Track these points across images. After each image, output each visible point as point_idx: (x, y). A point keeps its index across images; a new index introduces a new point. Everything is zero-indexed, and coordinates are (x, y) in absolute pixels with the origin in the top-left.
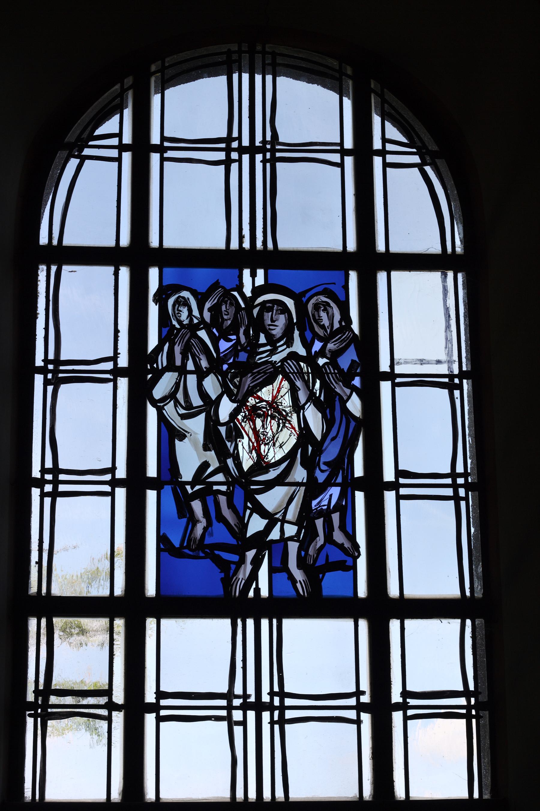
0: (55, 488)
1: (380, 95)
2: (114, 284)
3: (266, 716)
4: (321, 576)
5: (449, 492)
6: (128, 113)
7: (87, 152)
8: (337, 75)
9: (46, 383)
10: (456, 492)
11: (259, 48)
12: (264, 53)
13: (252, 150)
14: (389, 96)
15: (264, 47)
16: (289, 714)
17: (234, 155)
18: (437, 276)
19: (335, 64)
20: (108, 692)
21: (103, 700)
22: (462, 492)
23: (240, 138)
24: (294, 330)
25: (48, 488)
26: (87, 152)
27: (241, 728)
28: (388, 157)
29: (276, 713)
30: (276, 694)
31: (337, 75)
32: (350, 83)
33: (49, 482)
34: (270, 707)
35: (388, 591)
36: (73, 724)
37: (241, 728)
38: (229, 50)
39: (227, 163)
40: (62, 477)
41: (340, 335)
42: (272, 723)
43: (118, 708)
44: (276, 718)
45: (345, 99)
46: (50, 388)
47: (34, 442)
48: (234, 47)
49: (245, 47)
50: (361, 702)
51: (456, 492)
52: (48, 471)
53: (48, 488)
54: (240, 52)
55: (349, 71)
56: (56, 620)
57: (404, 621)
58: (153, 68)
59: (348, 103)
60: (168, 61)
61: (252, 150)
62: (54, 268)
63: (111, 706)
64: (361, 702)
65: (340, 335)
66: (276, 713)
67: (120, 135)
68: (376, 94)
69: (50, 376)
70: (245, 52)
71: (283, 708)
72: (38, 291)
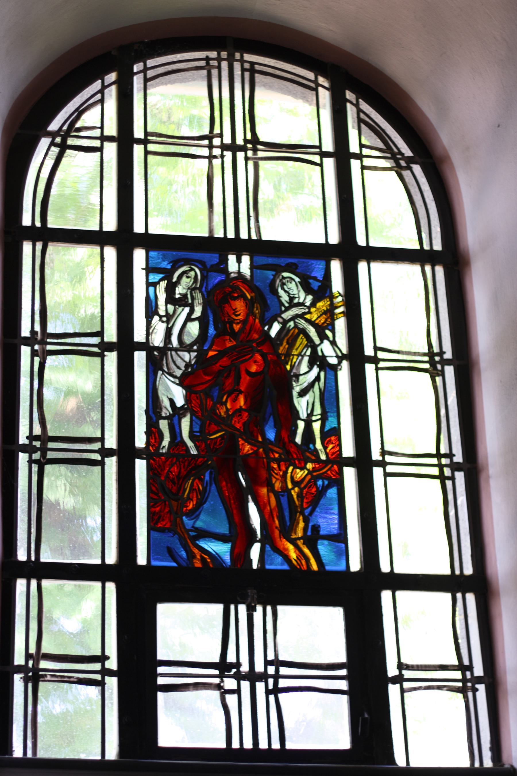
0: (44, 455)
2: (101, 113)
3: (260, 687)
5: (435, 471)
8: (313, 85)
9: (34, 354)
10: (441, 471)
11: (238, 56)
12: (242, 61)
13: (234, 148)
14: (364, 106)
15: (242, 56)
16: (283, 683)
17: (217, 152)
18: (416, 268)
19: (311, 75)
20: (103, 658)
22: (447, 472)
23: (221, 135)
24: (248, 502)
25: (36, 456)
27: (235, 696)
28: (364, 159)
29: (271, 681)
31: (313, 85)
34: (264, 677)
36: (61, 417)
37: (235, 696)
38: (207, 57)
39: (211, 157)
40: (51, 445)
42: (268, 692)
43: (111, 673)
44: (271, 687)
46: (37, 360)
47: (40, 736)
48: (213, 54)
49: (224, 54)
51: (441, 471)
52: (37, 438)
54: (219, 59)
58: (136, 68)
60: (150, 63)
61: (234, 148)
63: (106, 672)
66: (271, 681)
68: (351, 103)
69: (36, 347)
70: (224, 60)
71: (277, 677)
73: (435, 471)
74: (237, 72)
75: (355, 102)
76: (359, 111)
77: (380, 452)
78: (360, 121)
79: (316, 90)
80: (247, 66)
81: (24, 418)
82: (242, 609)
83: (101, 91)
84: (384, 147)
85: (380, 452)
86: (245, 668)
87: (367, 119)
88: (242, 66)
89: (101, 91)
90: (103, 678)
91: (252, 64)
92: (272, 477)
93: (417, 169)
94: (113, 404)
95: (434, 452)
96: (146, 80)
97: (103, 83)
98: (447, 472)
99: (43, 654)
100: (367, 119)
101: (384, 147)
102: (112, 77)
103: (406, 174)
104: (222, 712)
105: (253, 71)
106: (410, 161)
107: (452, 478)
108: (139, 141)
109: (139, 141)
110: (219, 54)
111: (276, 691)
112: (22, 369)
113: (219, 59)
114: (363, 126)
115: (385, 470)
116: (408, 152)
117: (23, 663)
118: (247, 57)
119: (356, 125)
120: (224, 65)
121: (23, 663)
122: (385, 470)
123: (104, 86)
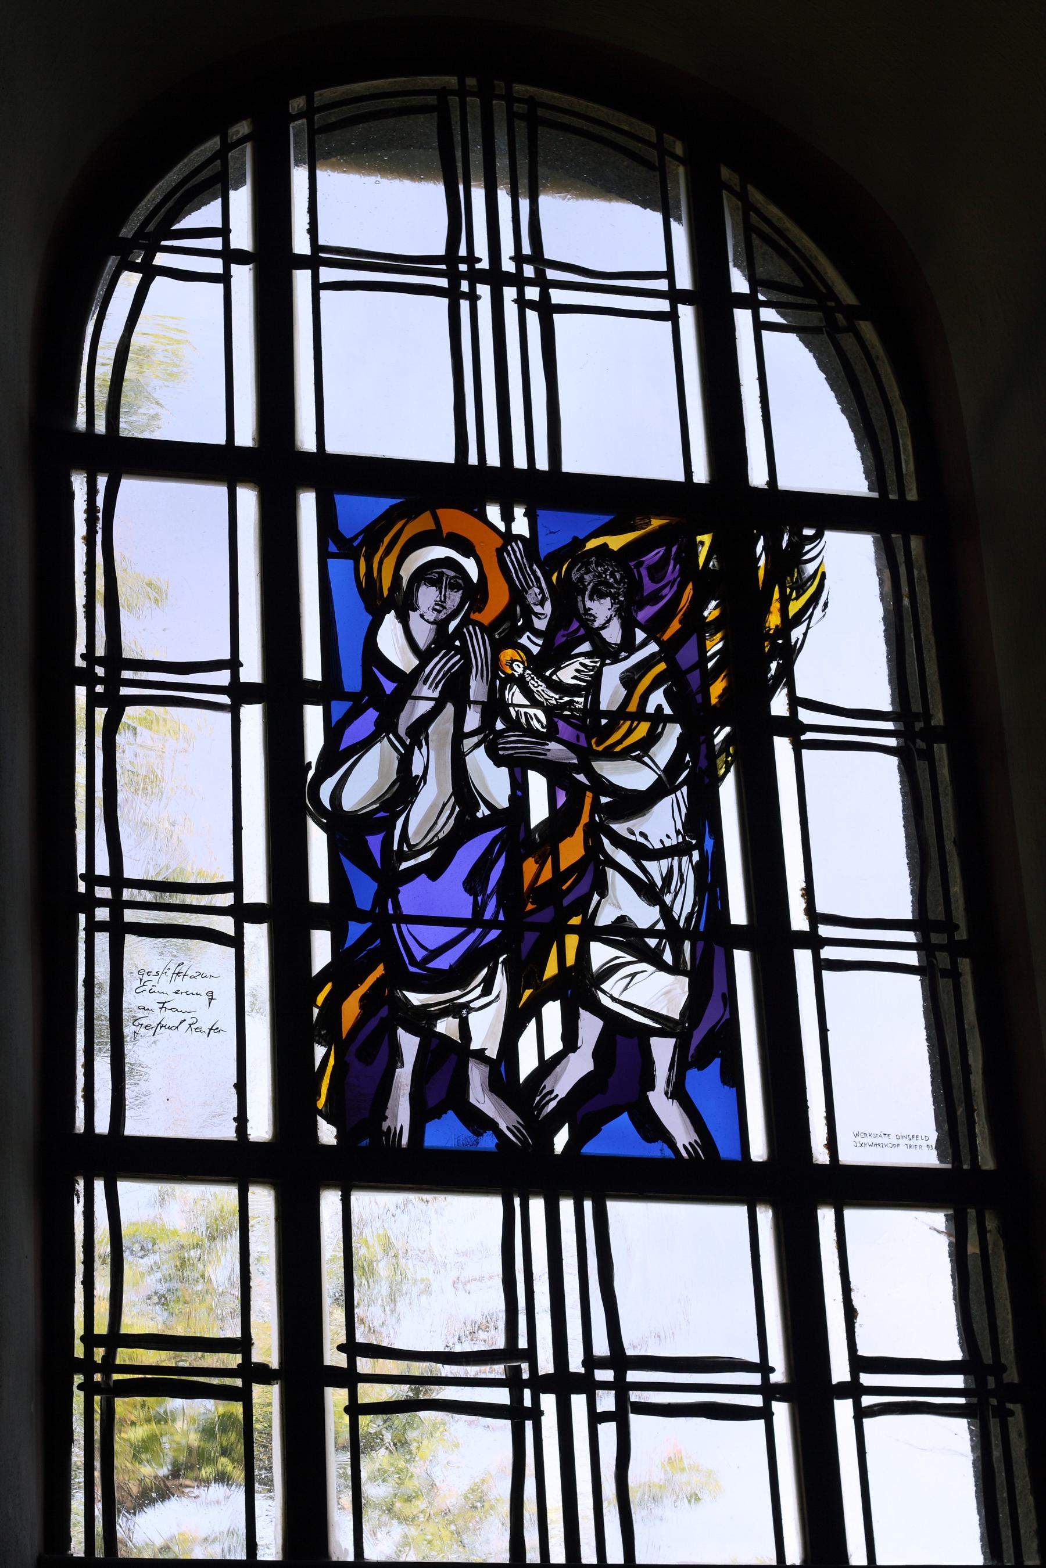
1: (742, 196)
3: (546, 1364)
4: (622, 722)
6: (241, 199)
7: (161, 259)
11: (500, 86)
12: (510, 99)
14: (756, 196)
15: (509, 89)
19: (649, 132)
21: (234, 1360)
26: (161, 259)
30: (464, 296)
32: (681, 170)
33: (103, 902)
35: (750, 478)
40: (127, 894)
41: (697, 962)
45: (674, 225)
50: (670, 322)
53: (102, 914)
54: (462, 92)
55: (679, 150)
56: (97, 1037)
57: (818, 1165)
59: (680, 233)
62: (102, 481)
64: (670, 322)
65: (697, 962)
67: (224, 232)
68: (731, 190)
72: (85, 610)
74: (511, 311)
75: (738, 189)
76: (748, 207)
78: (748, 231)
80: (519, 108)
81: (523, 1336)
83: (222, 154)
84: (797, 283)
86: (546, 1364)
87: (767, 229)
88: (510, 109)
89: (222, 154)
90: (352, 1362)
91: (532, 102)
92: (611, 873)
93: (866, 328)
96: (312, 132)
97: (224, 140)
100: (767, 229)
101: (797, 283)
104: (721, 1015)
105: (534, 123)
106: (852, 314)
108: (302, 262)
109: (302, 262)
110: (462, 82)
111: (509, 1353)
113: (462, 92)
114: (756, 241)
116: (848, 297)
117: (847, 1378)
118: (519, 89)
120: (474, 103)
121: (847, 1378)
123: (227, 147)
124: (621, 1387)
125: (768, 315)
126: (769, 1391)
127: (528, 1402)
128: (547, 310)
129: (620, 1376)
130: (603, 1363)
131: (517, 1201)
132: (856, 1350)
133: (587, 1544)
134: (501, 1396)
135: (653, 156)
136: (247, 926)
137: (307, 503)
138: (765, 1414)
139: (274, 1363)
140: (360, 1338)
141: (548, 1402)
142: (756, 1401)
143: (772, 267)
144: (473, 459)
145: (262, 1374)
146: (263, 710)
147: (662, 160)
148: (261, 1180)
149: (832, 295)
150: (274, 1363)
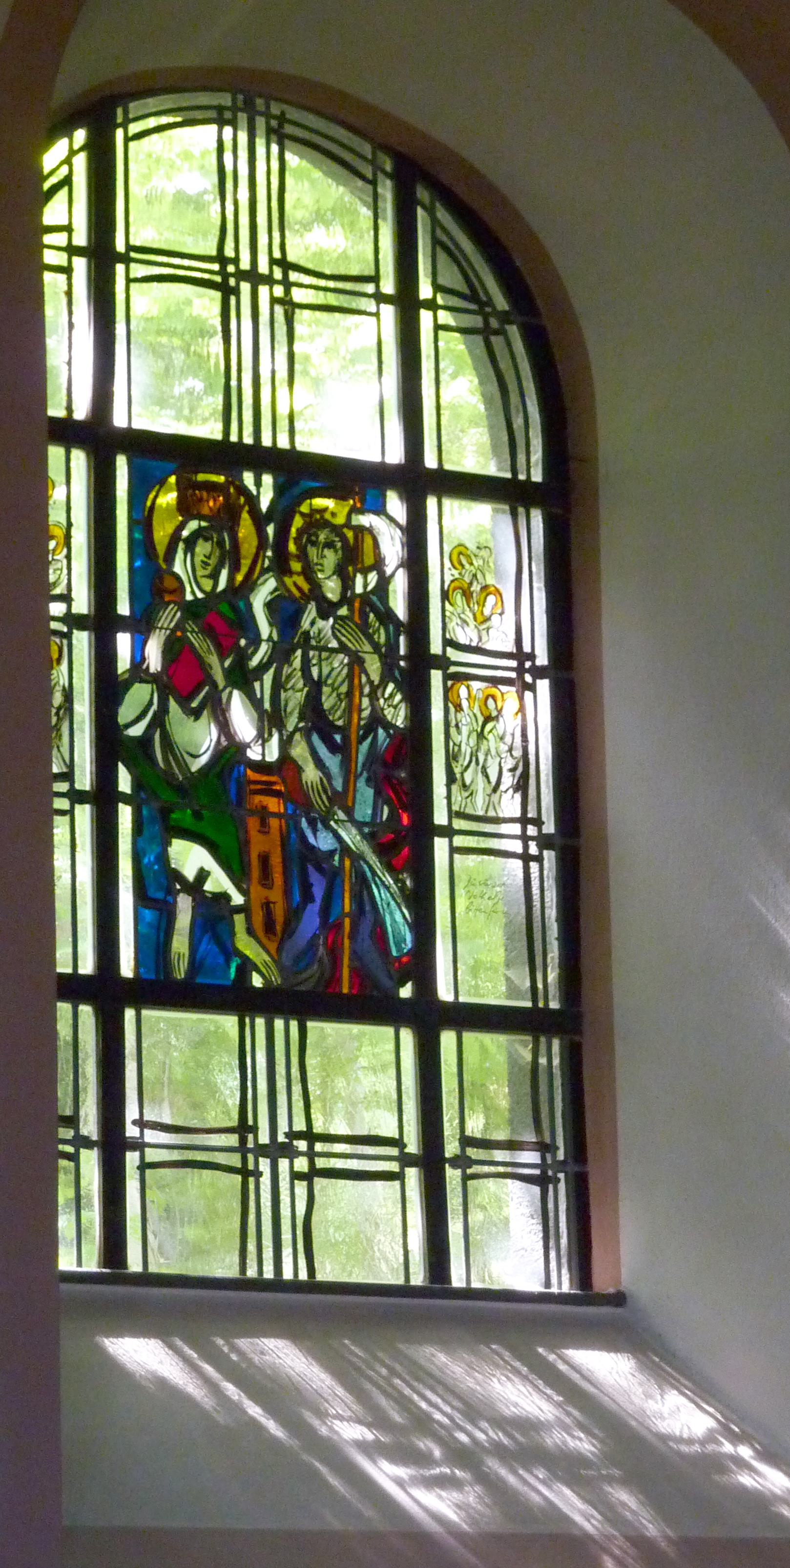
11: (260, 102)
12: (268, 116)
14: (442, 214)
15: (268, 107)
55: (388, 167)
68: (424, 207)
73: (517, 846)
76: (435, 223)
77: (193, 379)
78: (436, 242)
79: (373, 183)
82: (260, 1022)
84: (465, 290)
85: (193, 379)
87: (449, 244)
88: (268, 123)
94: (84, 700)
95: (214, 253)
98: (533, 849)
99: (240, 1274)
101: (465, 290)
102: (80, 136)
103: (497, 341)
107: (539, 859)
112: (121, 828)
115: (451, 842)
116: (501, 303)
119: (429, 249)
122: (451, 842)
124: (311, 1155)
125: (444, 317)
126: (406, 1160)
127: (251, 1166)
128: (290, 306)
129: (311, 1147)
130: (299, 1135)
131: (247, 1020)
132: (464, 1132)
133: (345, 1185)
134: (235, 1160)
135: (368, 172)
136: (82, 1150)
137: (122, 463)
138: (399, 1176)
139: (95, 1137)
140: (146, 1118)
141: (264, 1165)
142: (394, 1167)
143: (451, 277)
144: (234, 438)
145: (87, 1143)
146: (94, 368)
147: (375, 175)
148: (86, 1001)
149: (490, 302)
150: (95, 1137)
